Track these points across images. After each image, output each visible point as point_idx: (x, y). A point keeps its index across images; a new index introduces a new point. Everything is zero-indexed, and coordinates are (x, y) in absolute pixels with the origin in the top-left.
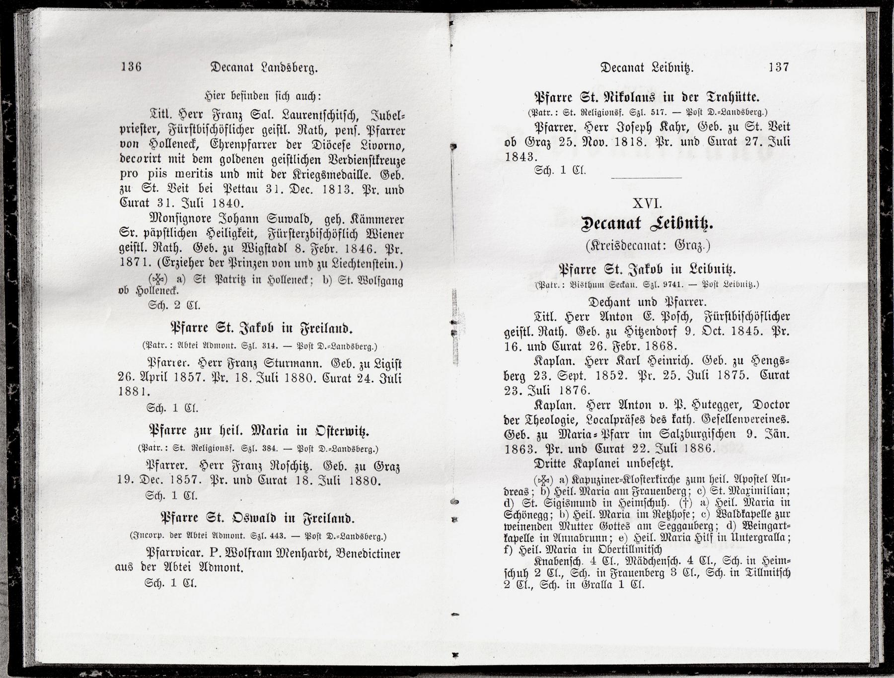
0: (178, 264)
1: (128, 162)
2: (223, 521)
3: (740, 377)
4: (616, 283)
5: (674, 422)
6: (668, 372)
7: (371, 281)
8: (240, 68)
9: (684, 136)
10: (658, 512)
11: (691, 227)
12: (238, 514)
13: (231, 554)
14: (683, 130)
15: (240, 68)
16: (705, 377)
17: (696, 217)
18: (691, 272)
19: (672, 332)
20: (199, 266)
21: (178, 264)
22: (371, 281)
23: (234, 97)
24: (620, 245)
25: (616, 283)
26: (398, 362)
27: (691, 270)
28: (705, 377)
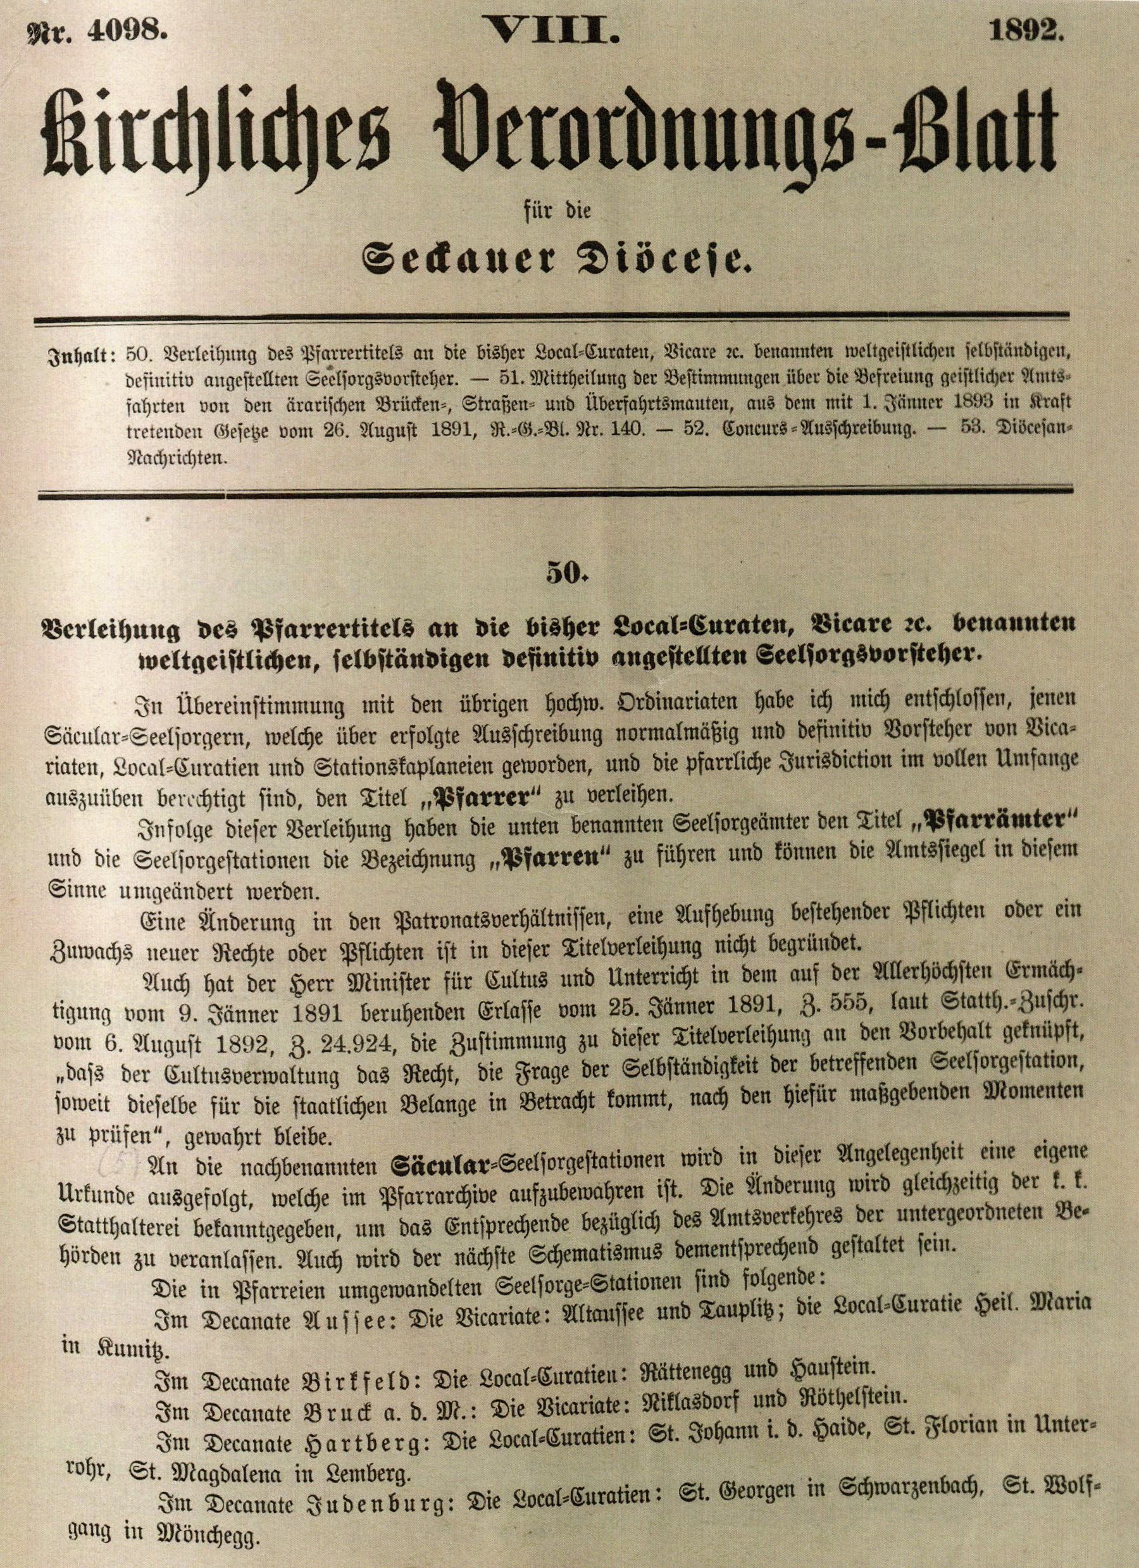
2: (680, 1196)
3: (832, 1007)
6: (376, 1040)
7: (1073, 1486)
9: (441, 417)
10: (415, 1069)
11: (180, 1388)
13: (1055, 1488)
14: (100, 1474)
17: (562, 648)
18: (517, 1505)
19: (731, 1402)
20: (421, 989)
22: (1073, 1486)
26: (669, 1184)
27: (516, 1502)
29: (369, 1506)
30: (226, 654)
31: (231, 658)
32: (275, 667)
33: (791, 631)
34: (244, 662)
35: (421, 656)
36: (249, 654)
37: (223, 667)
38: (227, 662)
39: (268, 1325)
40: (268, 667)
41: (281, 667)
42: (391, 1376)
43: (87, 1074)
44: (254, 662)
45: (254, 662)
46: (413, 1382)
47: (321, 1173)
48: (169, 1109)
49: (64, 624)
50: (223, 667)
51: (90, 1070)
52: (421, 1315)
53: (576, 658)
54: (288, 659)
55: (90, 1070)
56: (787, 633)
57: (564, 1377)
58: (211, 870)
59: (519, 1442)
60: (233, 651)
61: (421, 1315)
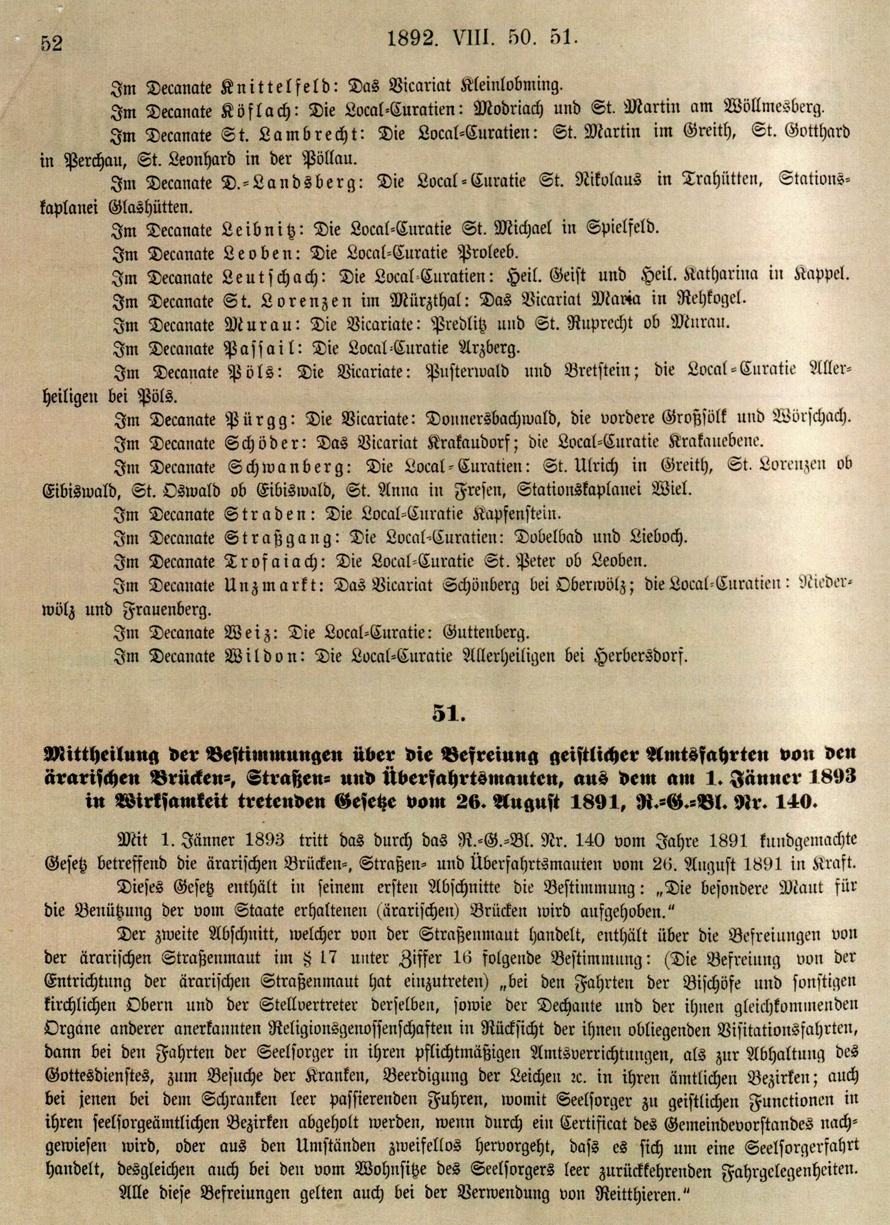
0: (430, 303)
1: (406, 1197)
4: (271, 1049)
5: (43, 213)
8: (654, 656)
12: (171, 486)
15: (654, 656)
16: (641, 938)
17: (498, 748)
21: (430, 303)
23: (96, 1054)
24: (653, 655)
25: (271, 1049)
28: (641, 938)
29: (295, 515)
30: (576, 750)
31: (579, 753)
32: (612, 759)
33: (561, 784)
34: (589, 756)
35: (361, 776)
36: (593, 750)
37: (573, 760)
38: (576, 756)
39: (195, 186)
40: (606, 760)
41: (617, 760)
42: (315, 82)
43: (586, 1147)
44: (596, 756)
45: (596, 756)
46: (332, 87)
47: (340, 1150)
48: (403, 1007)
49: (460, 751)
50: (573, 760)
51: (588, 1144)
52: (307, 369)
53: (81, 755)
54: (622, 754)
55: (588, 1144)
56: (558, 785)
57: (414, 253)
58: (666, 1037)
59: (372, 350)
60: (580, 748)
61: (307, 369)
